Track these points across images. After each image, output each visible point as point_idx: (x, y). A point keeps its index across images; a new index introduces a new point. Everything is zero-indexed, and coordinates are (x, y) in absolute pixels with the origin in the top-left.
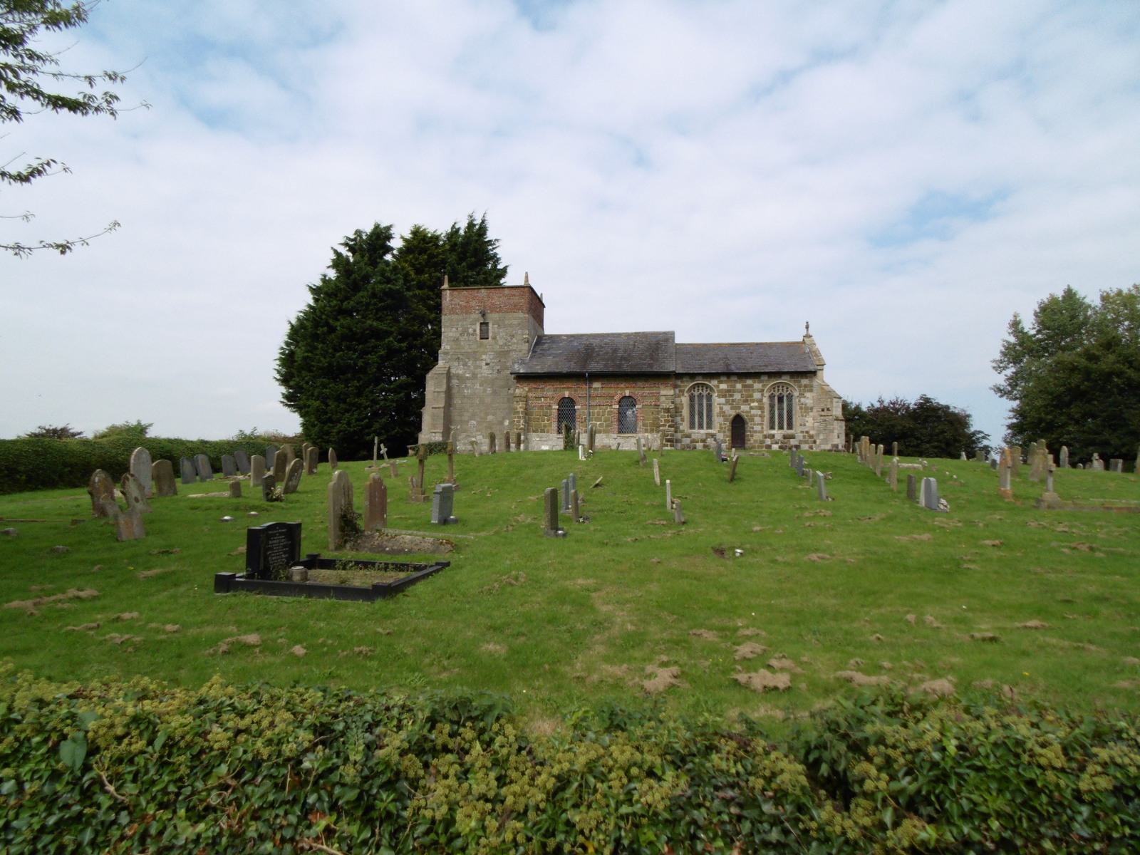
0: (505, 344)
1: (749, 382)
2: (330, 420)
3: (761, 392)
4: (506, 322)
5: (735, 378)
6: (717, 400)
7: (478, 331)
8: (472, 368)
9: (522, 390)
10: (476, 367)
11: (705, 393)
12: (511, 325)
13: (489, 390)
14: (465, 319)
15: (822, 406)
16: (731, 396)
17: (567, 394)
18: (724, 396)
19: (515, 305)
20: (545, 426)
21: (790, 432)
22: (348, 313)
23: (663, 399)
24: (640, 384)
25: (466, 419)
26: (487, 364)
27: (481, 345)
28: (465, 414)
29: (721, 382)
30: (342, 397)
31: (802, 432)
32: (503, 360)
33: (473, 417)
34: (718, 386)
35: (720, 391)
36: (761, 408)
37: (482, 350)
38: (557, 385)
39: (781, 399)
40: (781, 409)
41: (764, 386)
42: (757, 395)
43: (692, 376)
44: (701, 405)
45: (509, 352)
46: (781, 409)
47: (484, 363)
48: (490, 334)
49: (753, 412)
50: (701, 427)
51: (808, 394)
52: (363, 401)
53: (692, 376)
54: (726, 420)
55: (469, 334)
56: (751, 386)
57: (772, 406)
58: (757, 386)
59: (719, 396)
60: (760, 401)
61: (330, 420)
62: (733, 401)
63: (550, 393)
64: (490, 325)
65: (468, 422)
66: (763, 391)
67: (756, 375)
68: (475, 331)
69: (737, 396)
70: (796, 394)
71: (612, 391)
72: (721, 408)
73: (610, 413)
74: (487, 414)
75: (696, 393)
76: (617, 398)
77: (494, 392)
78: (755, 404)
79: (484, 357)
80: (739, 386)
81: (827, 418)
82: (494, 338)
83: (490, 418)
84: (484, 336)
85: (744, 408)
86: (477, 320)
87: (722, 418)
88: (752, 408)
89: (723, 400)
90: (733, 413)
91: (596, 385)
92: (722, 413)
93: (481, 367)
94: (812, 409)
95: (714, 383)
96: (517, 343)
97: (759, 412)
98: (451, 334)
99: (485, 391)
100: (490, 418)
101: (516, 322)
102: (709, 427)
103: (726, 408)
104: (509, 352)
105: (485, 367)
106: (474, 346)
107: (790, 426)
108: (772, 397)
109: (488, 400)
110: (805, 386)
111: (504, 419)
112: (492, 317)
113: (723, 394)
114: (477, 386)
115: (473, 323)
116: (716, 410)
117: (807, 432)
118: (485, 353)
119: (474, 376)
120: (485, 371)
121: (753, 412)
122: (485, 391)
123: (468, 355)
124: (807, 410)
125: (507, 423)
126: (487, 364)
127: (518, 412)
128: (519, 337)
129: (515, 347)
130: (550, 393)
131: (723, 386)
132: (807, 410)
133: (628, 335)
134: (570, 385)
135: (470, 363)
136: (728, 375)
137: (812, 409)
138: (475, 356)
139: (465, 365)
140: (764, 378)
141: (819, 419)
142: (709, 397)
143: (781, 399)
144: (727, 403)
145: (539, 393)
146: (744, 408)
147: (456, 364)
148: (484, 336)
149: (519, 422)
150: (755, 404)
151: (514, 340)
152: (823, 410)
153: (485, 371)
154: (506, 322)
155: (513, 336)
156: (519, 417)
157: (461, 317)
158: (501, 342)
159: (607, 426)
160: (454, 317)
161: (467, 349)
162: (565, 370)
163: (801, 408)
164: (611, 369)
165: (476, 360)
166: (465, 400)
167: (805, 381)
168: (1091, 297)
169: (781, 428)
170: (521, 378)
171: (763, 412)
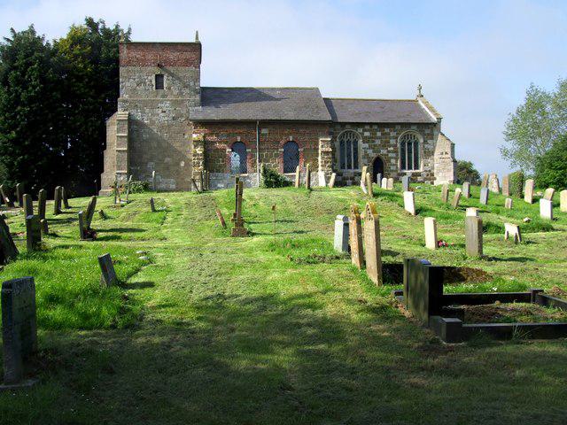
1: (387, 130)
16: (374, 142)
28: (145, 156)
34: (362, 134)
36: (396, 152)
39: (410, 144)
40: (410, 152)
42: (392, 142)
46: (410, 152)
49: (390, 155)
57: (403, 151)
66: (397, 138)
69: (378, 142)
76: (282, 142)
80: (379, 134)
82: (169, 89)
84: (159, 85)
85: (384, 152)
88: (389, 152)
89: (367, 145)
92: (366, 156)
97: (394, 155)
103: (370, 151)
108: (403, 144)
116: (361, 153)
121: (390, 155)
123: (146, 103)
126: (163, 112)
135: (147, 110)
142: (356, 143)
143: (410, 144)
146: (384, 152)
148: (159, 85)
163: (425, 152)
165: (152, 108)
167: (427, 131)
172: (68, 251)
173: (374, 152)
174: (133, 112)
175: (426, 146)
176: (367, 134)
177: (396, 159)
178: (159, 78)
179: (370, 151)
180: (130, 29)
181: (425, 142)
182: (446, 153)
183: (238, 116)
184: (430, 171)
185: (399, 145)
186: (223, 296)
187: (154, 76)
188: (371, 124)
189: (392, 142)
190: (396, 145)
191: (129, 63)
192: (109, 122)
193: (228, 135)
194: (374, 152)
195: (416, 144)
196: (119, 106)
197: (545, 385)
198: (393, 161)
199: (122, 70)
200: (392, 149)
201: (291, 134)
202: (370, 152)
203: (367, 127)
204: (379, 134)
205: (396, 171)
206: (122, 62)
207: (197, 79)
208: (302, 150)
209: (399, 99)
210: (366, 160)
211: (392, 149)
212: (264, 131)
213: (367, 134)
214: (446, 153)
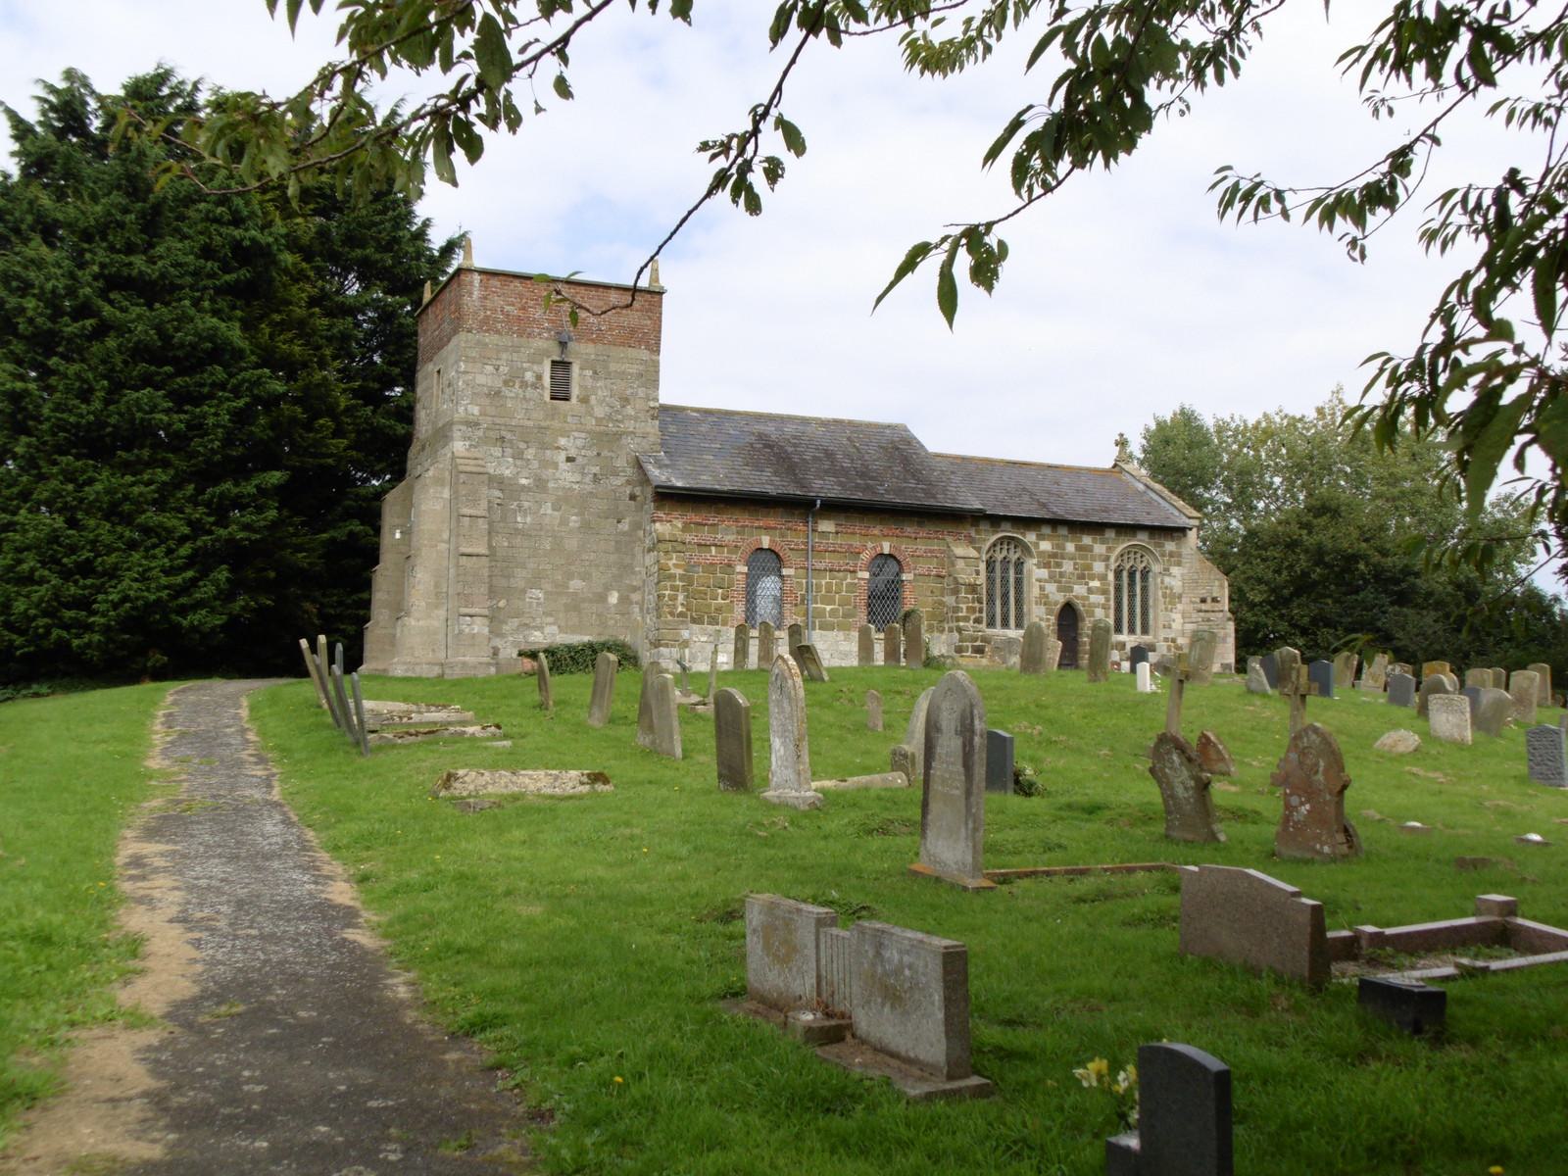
0: (609, 417)
1: (1087, 540)
2: (86, 569)
3: (1105, 555)
4: (613, 367)
5: (1063, 531)
6: (1035, 572)
7: (547, 380)
8: (535, 464)
9: (669, 525)
10: (546, 464)
11: (1013, 557)
12: (622, 375)
13: (574, 521)
14: (516, 349)
15: (1203, 593)
16: (1059, 565)
17: (766, 542)
18: (1047, 565)
19: (633, 331)
20: (719, 609)
21: (1148, 639)
22: (151, 291)
23: (960, 564)
24: (909, 530)
25: (521, 584)
26: (570, 459)
27: (553, 414)
28: (520, 573)
29: (1041, 537)
30: (127, 507)
31: (1166, 640)
32: (605, 453)
33: (535, 582)
34: (1037, 545)
35: (1041, 554)
36: (1105, 592)
37: (556, 424)
38: (745, 519)
39: (1132, 575)
40: (1132, 596)
41: (1109, 549)
42: (1099, 567)
43: (995, 520)
44: (1005, 580)
45: (618, 436)
46: (1132, 596)
47: (562, 456)
48: (575, 391)
49: (1093, 598)
50: (1005, 624)
51: (1175, 570)
52: (170, 520)
53: (995, 520)
54: (1049, 612)
55: (524, 385)
56: (1090, 549)
57: (1118, 589)
58: (1099, 549)
59: (1038, 566)
60: (1103, 578)
61: (86, 569)
62: (1062, 575)
63: (730, 538)
64: (575, 369)
65: (524, 591)
66: (1107, 559)
67: (1096, 528)
68: (539, 377)
69: (1068, 566)
70: (1156, 568)
71: (856, 542)
72: (1042, 588)
73: (852, 587)
74: (570, 576)
75: (999, 557)
76: (866, 556)
77: (586, 527)
78: (1095, 584)
79: (562, 441)
80: (1070, 547)
81: (1212, 616)
82: (584, 400)
83: (576, 584)
84: (560, 394)
85: (1079, 590)
86: (546, 353)
87: (1043, 608)
88: (1090, 591)
89: (1044, 573)
90: (1060, 599)
91: (826, 526)
92: (1044, 600)
93: (556, 466)
94: (1180, 597)
95: (1030, 537)
96: (636, 419)
97: (1101, 599)
98: (481, 379)
99: (564, 522)
100: (576, 584)
101: (634, 369)
102: (1145, 630)
103: (1051, 588)
104: (618, 436)
105: (564, 466)
106: (538, 415)
107: (1145, 630)
108: (1118, 574)
109: (572, 544)
110: (1171, 554)
111: (607, 588)
112: (581, 352)
113: (1050, 561)
114: (547, 509)
115: (536, 359)
116: (1033, 591)
117: (1174, 640)
118: (566, 434)
119: (540, 484)
120: (566, 476)
121: (1093, 598)
122: (564, 522)
123: (526, 434)
124: (1173, 598)
125: (613, 598)
126: (570, 459)
127: (672, 577)
128: (640, 404)
129: (630, 425)
130: (730, 538)
131: (1046, 546)
132: (1173, 598)
133: (824, 423)
134: (772, 522)
135: (530, 453)
136: (1055, 523)
137: (1180, 597)
138: (540, 437)
139: (518, 456)
140: (1110, 534)
141: (1196, 617)
142: (1019, 564)
143: (1132, 575)
144: (1052, 578)
145: (705, 535)
146: (1079, 590)
147: (497, 451)
148: (560, 394)
149: (674, 598)
150: (1095, 584)
151: (629, 410)
152: (1203, 601)
153: (566, 476)
154: (613, 367)
155: (625, 401)
156: (674, 588)
157: (506, 341)
158: (600, 411)
159: (845, 616)
160: (491, 339)
161: (519, 418)
162: (727, 486)
163: (1164, 596)
164: (859, 495)
165: (543, 446)
166: (518, 541)
167: (1170, 546)
168: (1209, 422)
169: (1132, 631)
170: (669, 498)
171: (1108, 600)
173: (1059, 590)
175: (1167, 579)
177: (1105, 607)
178: (561, 366)
185: (1111, 577)
191: (486, 325)
194: (1059, 590)
197: (396, 891)
202: (1051, 588)
203: (1046, 530)
204: (1070, 547)
207: (650, 377)
208: (860, 574)
209: (1066, 463)
214: (1215, 600)
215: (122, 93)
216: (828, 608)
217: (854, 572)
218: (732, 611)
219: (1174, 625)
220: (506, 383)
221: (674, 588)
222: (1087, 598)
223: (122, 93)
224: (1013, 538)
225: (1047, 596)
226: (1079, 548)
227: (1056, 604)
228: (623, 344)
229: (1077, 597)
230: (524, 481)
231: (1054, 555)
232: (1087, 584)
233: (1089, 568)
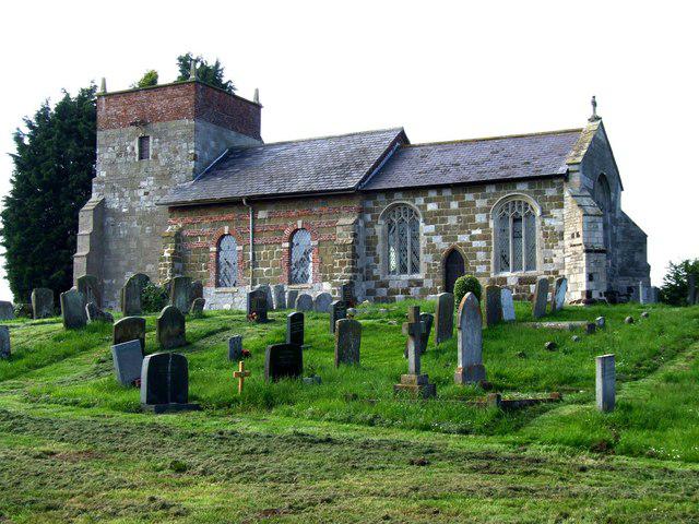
1: (469, 197)
3: (484, 213)
5: (447, 193)
16: (444, 220)
25: (123, 269)
28: (122, 263)
36: (485, 237)
41: (490, 202)
42: (480, 218)
49: (476, 244)
58: (481, 203)
62: (447, 228)
68: (133, 149)
69: (452, 220)
71: (281, 223)
72: (429, 241)
78: (478, 232)
80: (454, 205)
82: (155, 157)
84: (143, 155)
85: (463, 238)
88: (473, 238)
89: (431, 228)
90: (442, 245)
92: (431, 248)
97: (483, 244)
105: (144, 198)
121: (476, 244)
122: (143, 231)
126: (146, 194)
140: (491, 190)
146: (463, 238)
157: (117, 131)
163: (545, 235)
167: (551, 192)
171: (490, 244)
172: (387, 352)
173: (444, 240)
174: (109, 196)
175: (547, 221)
176: (432, 207)
177: (487, 250)
178: (143, 140)
179: (437, 240)
180: (104, 80)
181: (545, 214)
182: (578, 236)
183: (218, 196)
184: (556, 273)
186: (650, 428)
187: (137, 139)
188: (439, 188)
189: (480, 218)
190: (487, 225)
192: (81, 214)
193: (213, 225)
194: (444, 240)
195: (530, 216)
196: (94, 189)
198: (481, 256)
199: (100, 136)
200: (479, 232)
201: (299, 216)
203: (433, 194)
204: (454, 205)
205: (487, 275)
206: (100, 125)
210: (430, 256)
211: (479, 232)
212: (262, 214)
213: (432, 207)
215: (224, 81)
216: (265, 270)
217: (280, 243)
218: (209, 276)
219: (555, 260)
220: (118, 155)
221: (165, 266)
222: (470, 244)
223: (224, 81)
224: (397, 205)
225: (434, 246)
226: (461, 205)
227: (442, 251)
228: (174, 119)
229: (461, 245)
230: (124, 210)
231: (438, 213)
232: (469, 233)
233: (472, 219)
